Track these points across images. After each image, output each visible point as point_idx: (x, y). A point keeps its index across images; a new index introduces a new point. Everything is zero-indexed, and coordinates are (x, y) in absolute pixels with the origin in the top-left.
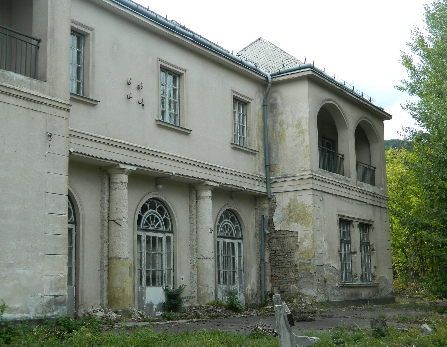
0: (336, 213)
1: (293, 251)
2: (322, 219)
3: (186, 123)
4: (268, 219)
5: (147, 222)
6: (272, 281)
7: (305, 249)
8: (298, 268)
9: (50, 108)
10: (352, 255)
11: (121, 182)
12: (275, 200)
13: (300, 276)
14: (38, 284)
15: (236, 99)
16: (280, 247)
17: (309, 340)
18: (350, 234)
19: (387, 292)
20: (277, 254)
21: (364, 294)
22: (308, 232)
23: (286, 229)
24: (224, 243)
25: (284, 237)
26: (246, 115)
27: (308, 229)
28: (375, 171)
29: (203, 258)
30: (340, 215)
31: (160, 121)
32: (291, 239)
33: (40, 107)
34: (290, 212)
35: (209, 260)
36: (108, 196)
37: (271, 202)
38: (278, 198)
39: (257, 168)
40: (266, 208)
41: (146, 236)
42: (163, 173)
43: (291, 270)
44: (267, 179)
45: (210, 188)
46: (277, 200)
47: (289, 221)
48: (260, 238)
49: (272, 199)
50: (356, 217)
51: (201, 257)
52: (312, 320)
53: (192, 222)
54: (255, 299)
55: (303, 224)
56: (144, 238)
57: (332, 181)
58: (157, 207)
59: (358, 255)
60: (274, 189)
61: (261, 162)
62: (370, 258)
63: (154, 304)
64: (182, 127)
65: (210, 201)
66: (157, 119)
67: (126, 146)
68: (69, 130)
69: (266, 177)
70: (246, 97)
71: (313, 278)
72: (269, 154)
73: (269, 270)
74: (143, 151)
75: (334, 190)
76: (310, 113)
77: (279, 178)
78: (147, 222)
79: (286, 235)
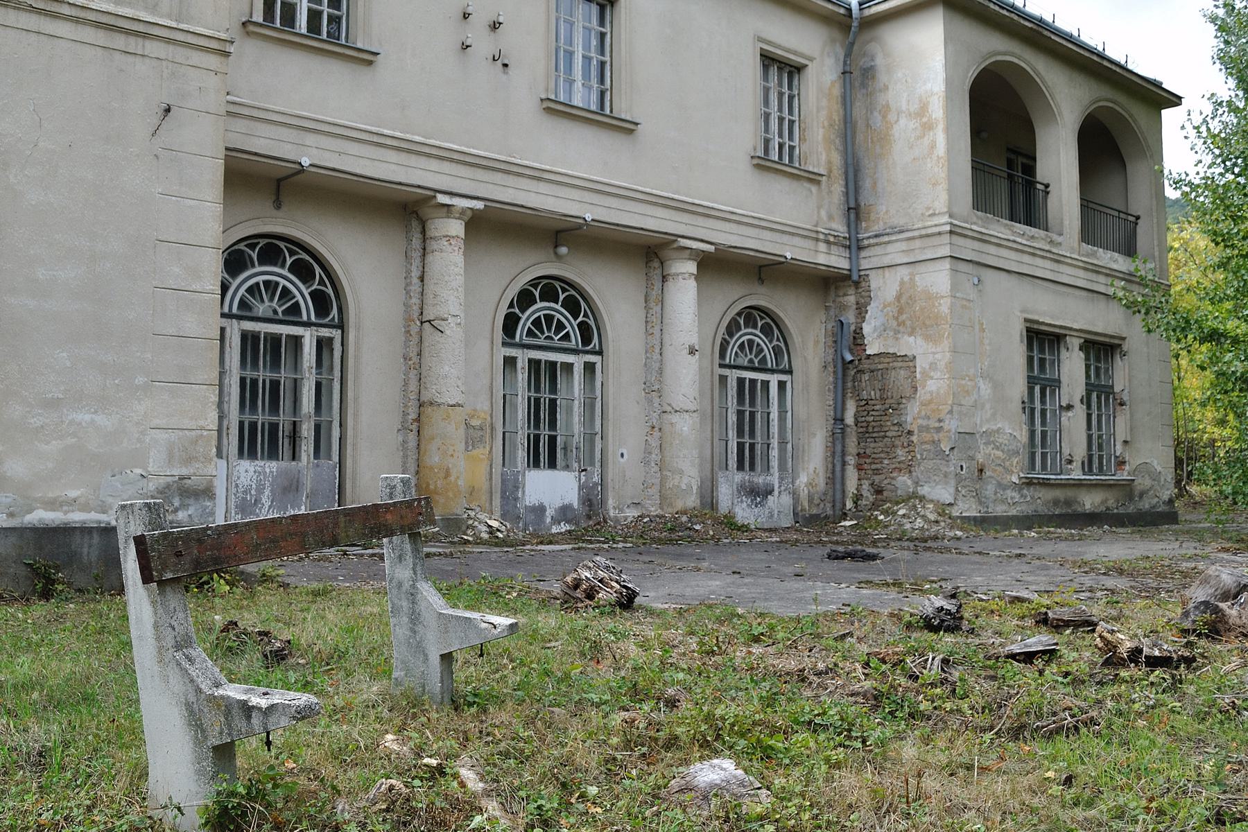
0: (1019, 314)
1: (904, 401)
2: (977, 327)
3: (623, 108)
4: (853, 328)
5: (533, 328)
6: (859, 468)
7: (931, 395)
8: (914, 438)
9: (171, 48)
10: (1064, 414)
11: (447, 236)
12: (869, 286)
13: (919, 456)
14: (134, 447)
15: (769, 60)
16: (878, 392)
17: (476, 627)
18: (1059, 366)
19: (1157, 499)
20: (870, 408)
21: (1090, 501)
22: (938, 356)
23: (891, 351)
24: (741, 381)
25: (887, 369)
26: (799, 94)
27: (939, 349)
28: (1137, 224)
29: (673, 411)
30: (1026, 320)
31: (759, 157)
32: (902, 372)
33: (143, 46)
34: (901, 311)
35: (686, 416)
36: (421, 269)
37: (860, 290)
38: (875, 281)
39: (823, 213)
40: (849, 304)
41: (529, 359)
42: (558, 217)
43: (900, 443)
44: (849, 239)
45: (690, 255)
46: (873, 285)
47: (897, 332)
48: (834, 372)
49: (863, 284)
50: (1076, 326)
51: (669, 409)
52: (873, 557)
53: (651, 331)
54: (818, 505)
55: (927, 338)
56: (522, 364)
57: (1009, 240)
58: (562, 297)
59: (1080, 411)
60: (866, 261)
61: (836, 201)
62: (1114, 422)
63: (548, 507)
64: (616, 116)
65: (692, 284)
66: (543, 97)
67: (455, 156)
68: (227, 102)
69: (849, 232)
70: (795, 53)
71: (948, 461)
72: (856, 183)
73: (853, 442)
74: (503, 166)
75: (1013, 262)
76: (949, 82)
77: (876, 236)
78: (533, 328)
79: (891, 364)
